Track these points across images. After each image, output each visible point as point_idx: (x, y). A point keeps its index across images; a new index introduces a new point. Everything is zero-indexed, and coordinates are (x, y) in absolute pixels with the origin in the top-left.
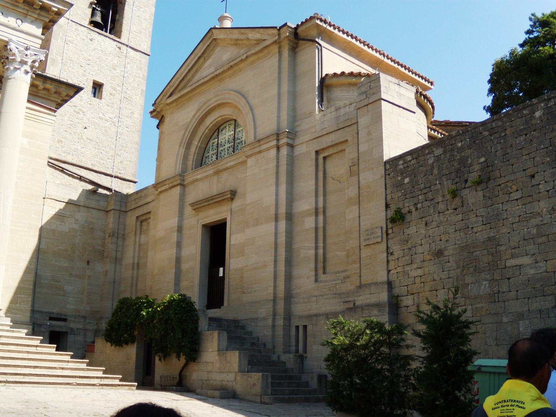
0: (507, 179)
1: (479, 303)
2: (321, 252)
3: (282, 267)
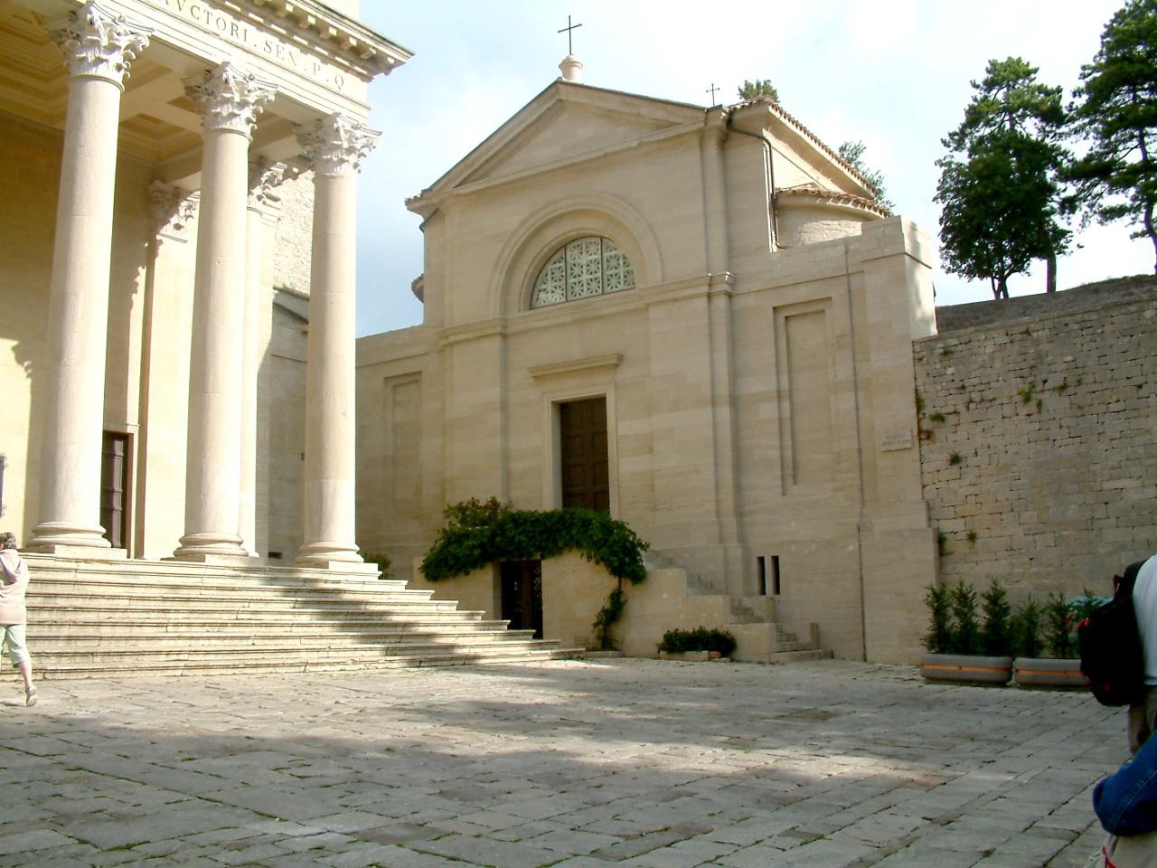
0: (1105, 386)
1: (1065, 530)
2: (789, 453)
3: (727, 474)
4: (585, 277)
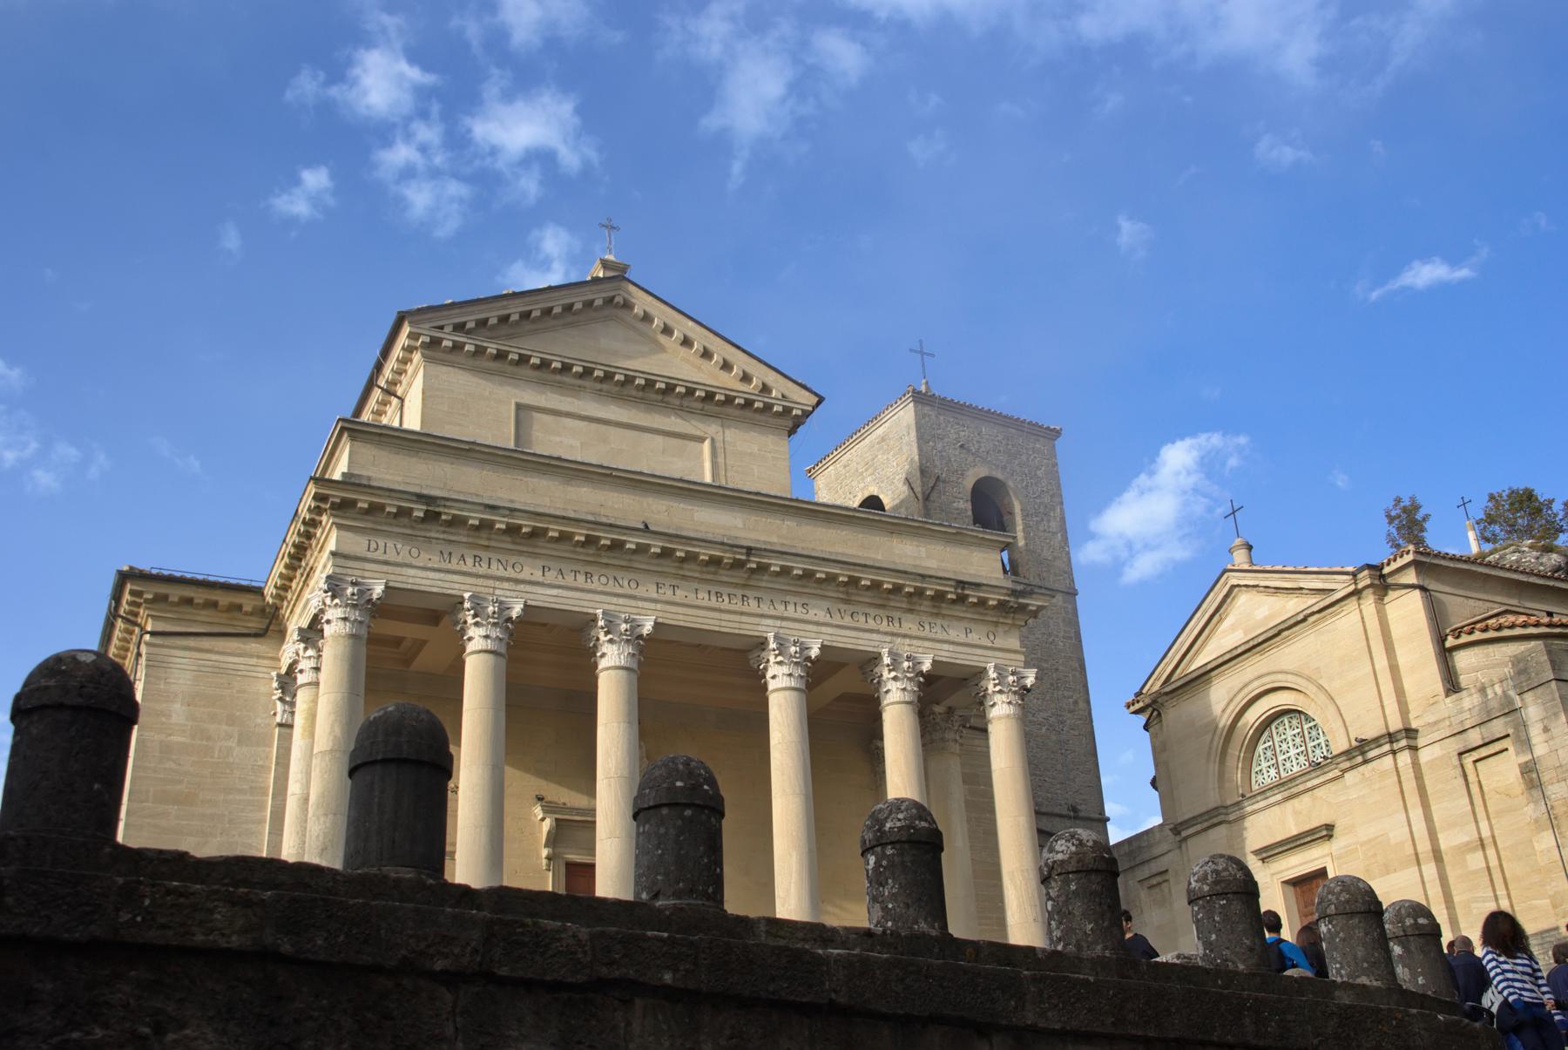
4: (1293, 752)
